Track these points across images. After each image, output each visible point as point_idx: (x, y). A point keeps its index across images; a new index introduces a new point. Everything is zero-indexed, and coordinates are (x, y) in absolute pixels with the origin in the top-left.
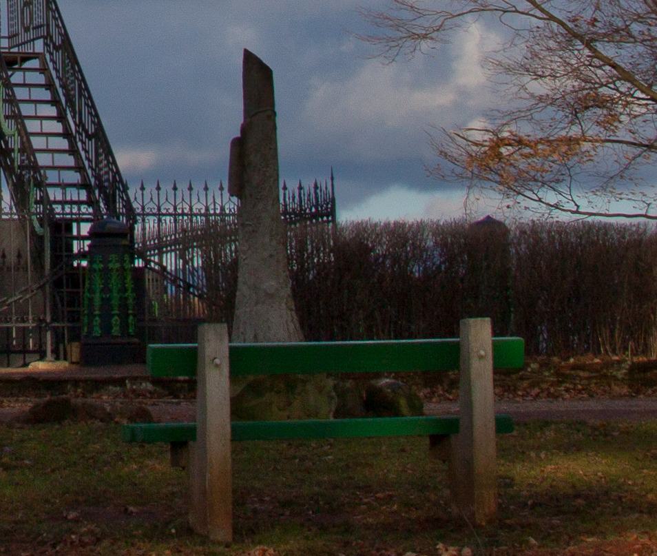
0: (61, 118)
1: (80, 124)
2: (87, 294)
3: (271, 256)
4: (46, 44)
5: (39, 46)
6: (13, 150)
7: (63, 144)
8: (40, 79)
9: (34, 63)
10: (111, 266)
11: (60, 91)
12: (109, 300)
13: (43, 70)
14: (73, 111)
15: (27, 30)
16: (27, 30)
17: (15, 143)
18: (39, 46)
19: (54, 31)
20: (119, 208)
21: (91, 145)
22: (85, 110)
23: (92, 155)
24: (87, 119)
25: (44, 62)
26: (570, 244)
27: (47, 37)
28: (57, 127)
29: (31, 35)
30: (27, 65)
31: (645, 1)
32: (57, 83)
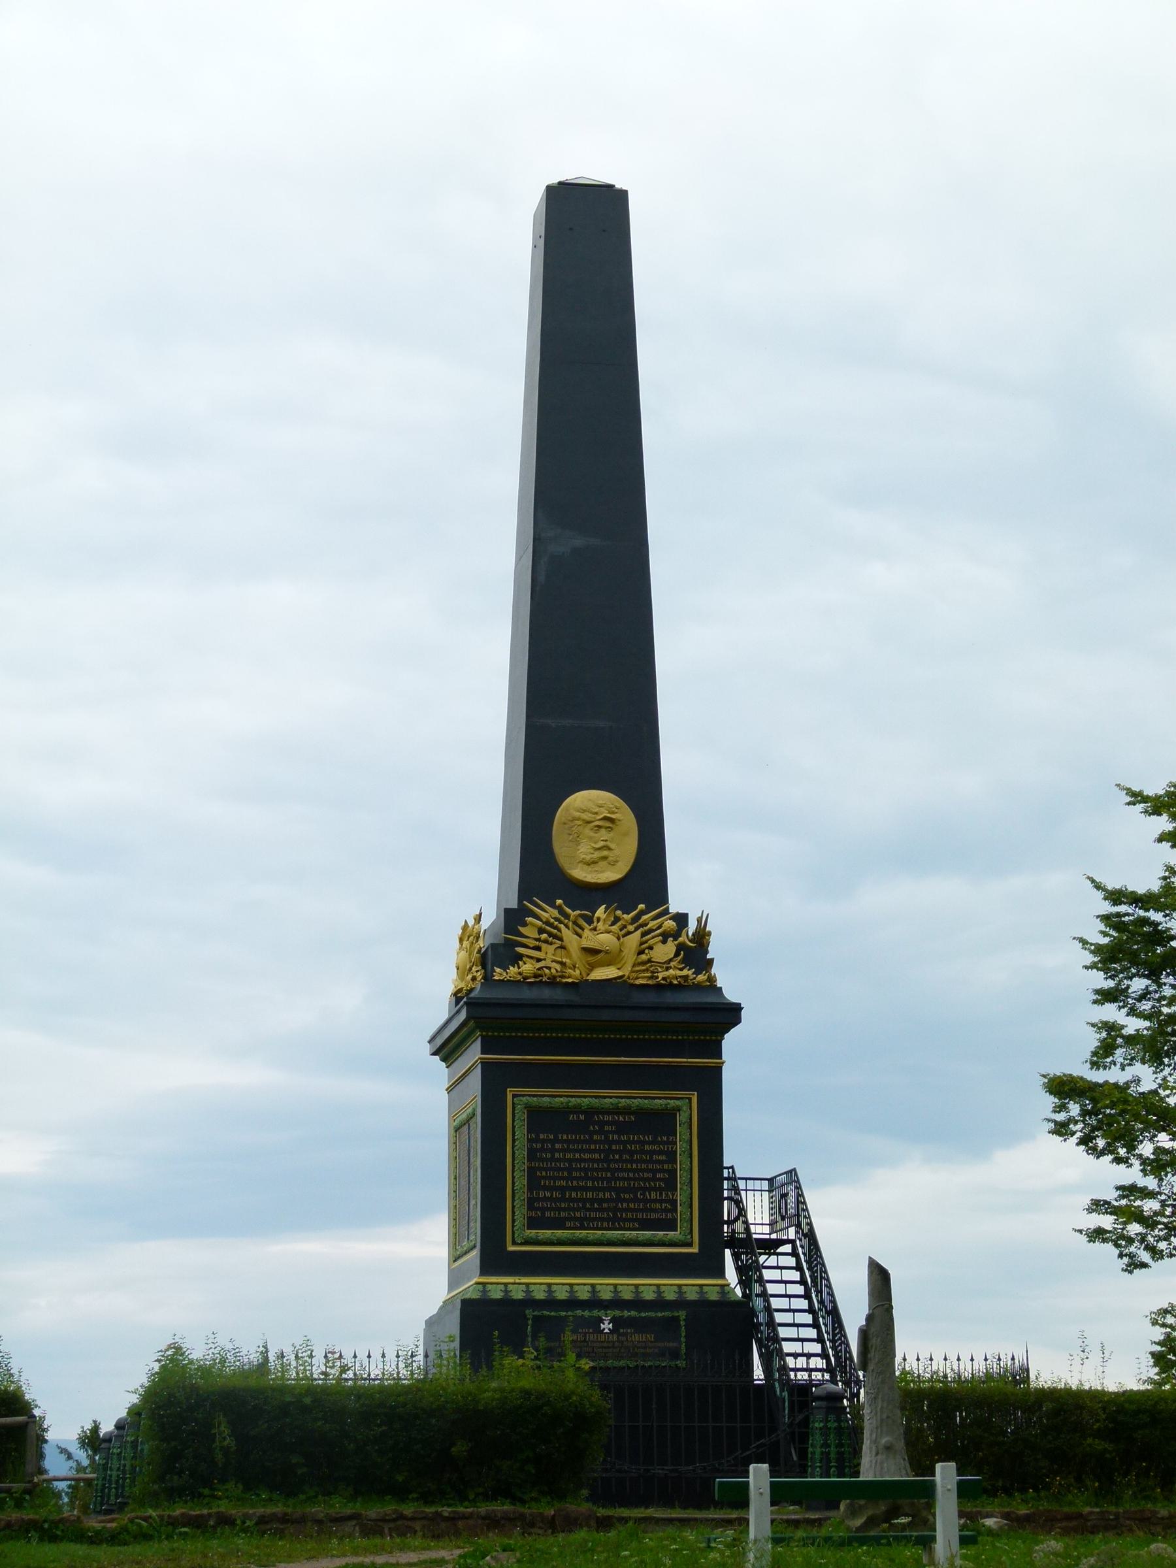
0: (807, 1296)
1: (821, 1302)
2: (810, 1449)
3: (888, 1417)
4: (797, 1232)
5: (792, 1233)
6: (761, 1324)
7: (808, 1318)
8: (792, 1261)
9: (787, 1248)
10: (829, 1425)
11: (807, 1273)
12: (828, 1453)
13: (794, 1253)
14: (817, 1292)
15: (783, 1218)
16: (783, 1218)
17: (762, 1318)
18: (792, 1233)
19: (804, 1222)
20: (809, 1370)
21: (829, 1320)
22: (825, 1291)
23: (830, 1328)
24: (827, 1299)
25: (794, 1248)
26: (557, 1344)
27: (798, 1226)
28: (804, 1304)
29: (786, 1223)
30: (781, 1249)
31: (1175, 1401)
32: (805, 1265)
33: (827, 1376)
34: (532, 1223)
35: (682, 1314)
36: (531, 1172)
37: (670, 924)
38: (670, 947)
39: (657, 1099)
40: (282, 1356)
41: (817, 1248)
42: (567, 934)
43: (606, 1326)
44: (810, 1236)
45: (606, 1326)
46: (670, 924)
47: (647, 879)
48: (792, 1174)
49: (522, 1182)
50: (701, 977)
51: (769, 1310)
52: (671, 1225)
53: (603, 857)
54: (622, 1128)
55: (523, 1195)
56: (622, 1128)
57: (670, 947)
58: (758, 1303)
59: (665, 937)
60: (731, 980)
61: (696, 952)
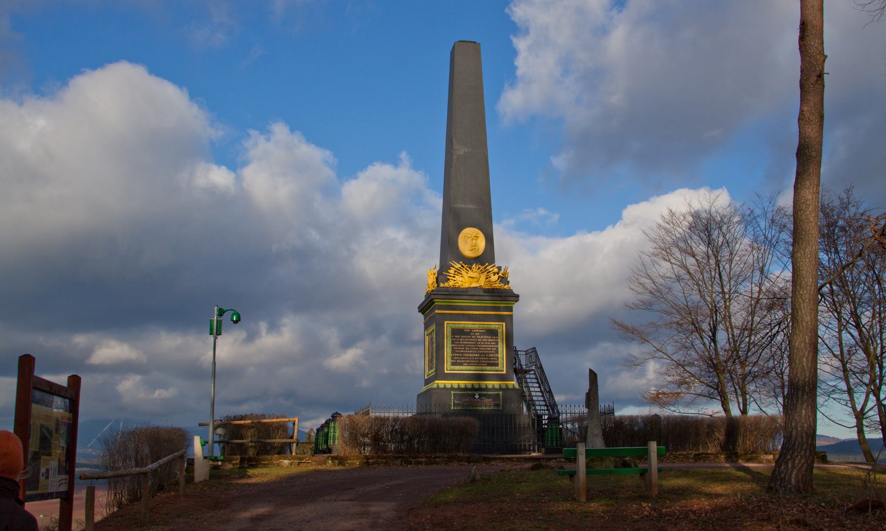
0: (539, 387)
5: (534, 368)
7: (540, 394)
13: (535, 374)
17: (527, 394)
18: (534, 368)
28: (539, 390)
33: (513, 383)
34: (453, 364)
35: (501, 393)
36: (453, 348)
37: (496, 270)
38: (496, 277)
39: (494, 325)
40: (656, 248)
41: (543, 371)
42: (463, 272)
43: (477, 397)
44: (541, 367)
45: (477, 397)
46: (496, 270)
47: (486, 258)
48: (534, 350)
49: (449, 350)
50: (506, 287)
51: (530, 392)
52: (497, 365)
53: (474, 248)
54: (481, 334)
55: (450, 355)
56: (481, 334)
57: (496, 277)
58: (525, 390)
59: (494, 274)
60: (515, 285)
61: (504, 279)
